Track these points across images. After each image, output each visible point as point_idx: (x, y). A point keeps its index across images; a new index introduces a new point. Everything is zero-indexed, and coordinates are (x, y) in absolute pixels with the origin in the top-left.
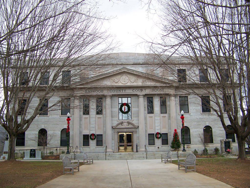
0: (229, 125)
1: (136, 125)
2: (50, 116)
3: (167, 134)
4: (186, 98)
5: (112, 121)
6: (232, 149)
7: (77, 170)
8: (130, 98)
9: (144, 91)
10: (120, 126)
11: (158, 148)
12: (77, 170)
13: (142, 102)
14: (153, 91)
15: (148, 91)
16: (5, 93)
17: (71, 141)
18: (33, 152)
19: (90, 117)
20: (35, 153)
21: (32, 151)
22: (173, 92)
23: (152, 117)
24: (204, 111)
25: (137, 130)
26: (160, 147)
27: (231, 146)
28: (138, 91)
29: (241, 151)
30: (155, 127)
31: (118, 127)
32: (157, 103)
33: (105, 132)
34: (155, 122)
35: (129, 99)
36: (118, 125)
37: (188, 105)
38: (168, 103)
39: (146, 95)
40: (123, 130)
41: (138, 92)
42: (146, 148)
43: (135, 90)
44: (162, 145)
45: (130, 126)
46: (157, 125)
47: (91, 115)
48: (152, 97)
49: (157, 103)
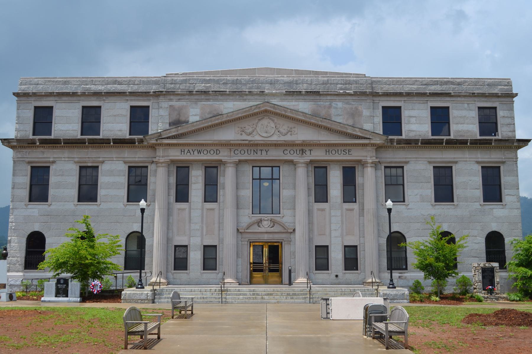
4: (399, 170)
9: (308, 153)
11: (335, 278)
15: (319, 155)
18: (63, 284)
21: (61, 284)
23: (323, 210)
25: (292, 236)
26: (340, 275)
33: (221, 241)
37: (403, 185)
39: (311, 162)
43: (288, 152)
45: (276, 229)
46: (333, 227)
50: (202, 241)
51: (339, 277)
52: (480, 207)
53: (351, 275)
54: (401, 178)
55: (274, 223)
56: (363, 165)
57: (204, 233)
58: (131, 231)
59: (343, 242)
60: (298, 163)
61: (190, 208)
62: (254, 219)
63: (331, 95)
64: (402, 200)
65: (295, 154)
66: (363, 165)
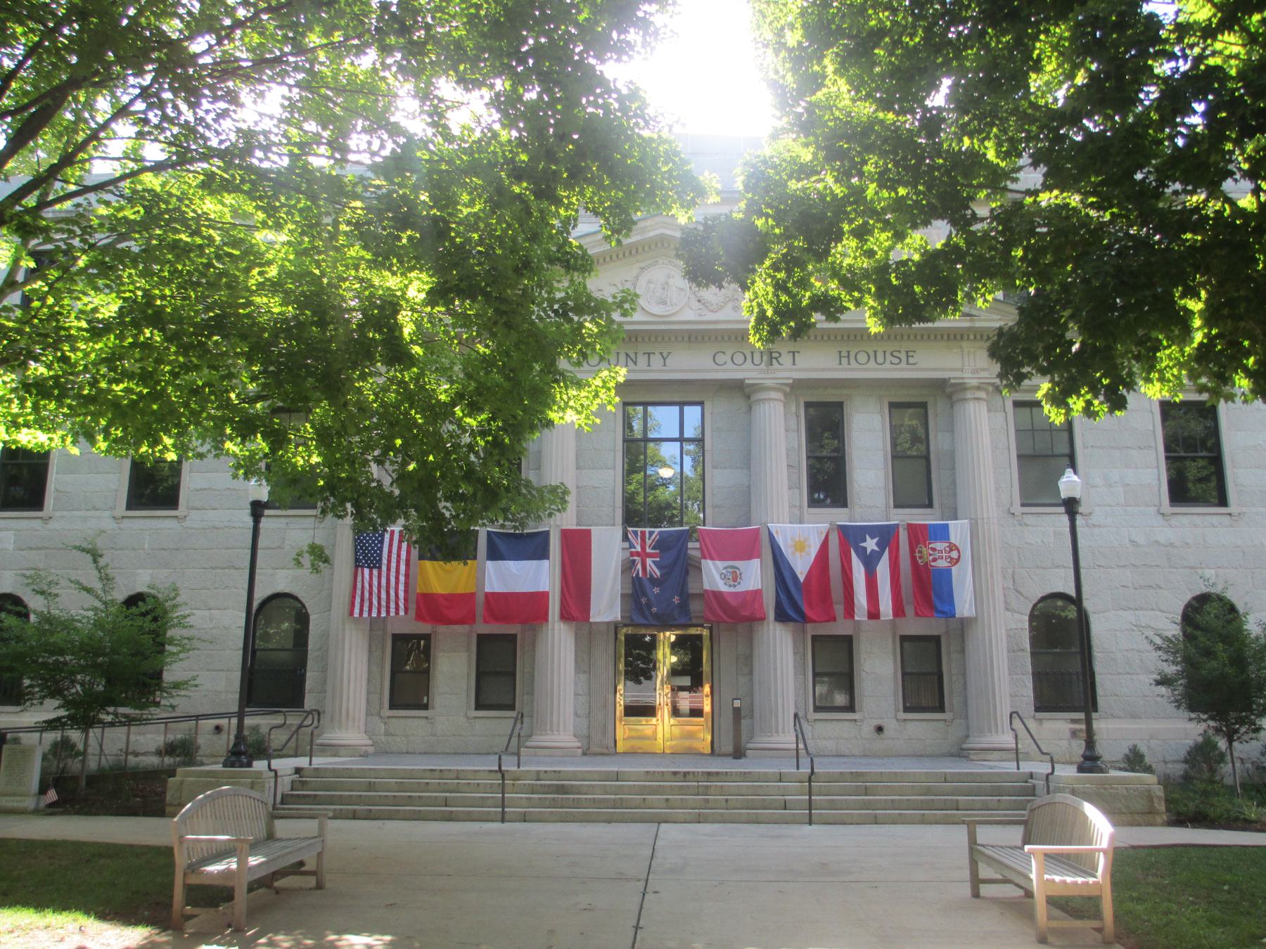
0: (1055, 590)
2: (193, 514)
7: (312, 881)
8: (699, 408)
9: (786, 359)
12: (312, 881)
14: (844, 360)
17: (312, 677)
22: (975, 371)
24: (1180, 492)
26: (891, 726)
28: (872, 359)
29: (224, 854)
35: (693, 413)
38: (938, 441)
39: (797, 386)
41: (749, 364)
42: (800, 735)
43: (727, 358)
44: (902, 715)
48: (840, 405)
56: (950, 397)
65: (872, 364)
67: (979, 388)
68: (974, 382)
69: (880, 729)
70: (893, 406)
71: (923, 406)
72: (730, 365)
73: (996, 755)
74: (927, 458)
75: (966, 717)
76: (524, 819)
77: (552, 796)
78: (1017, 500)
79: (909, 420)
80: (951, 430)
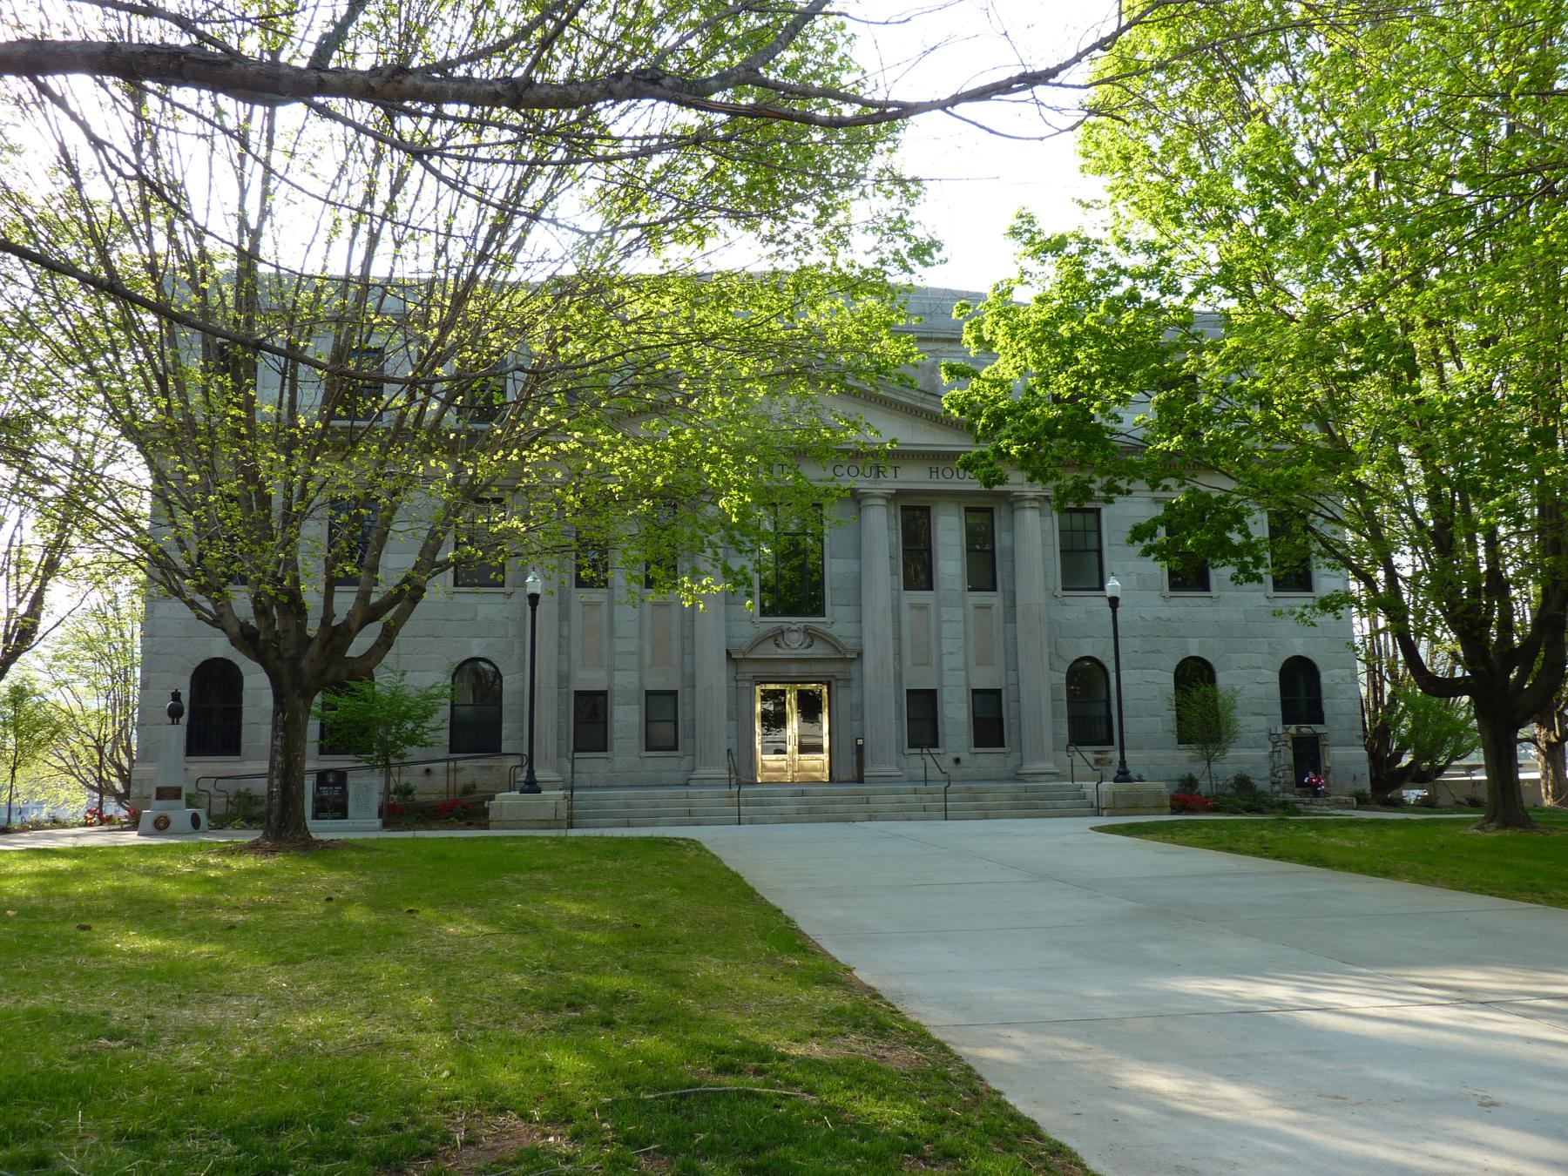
1: (850, 643)
3: (998, 692)
4: (1090, 518)
5: (727, 620)
6: (1327, 772)
9: (890, 473)
10: (769, 651)
11: (953, 764)
13: (881, 528)
15: (914, 478)
16: (86, 44)
18: (333, 785)
19: (611, 603)
20: (344, 793)
21: (328, 785)
23: (923, 607)
25: (854, 668)
26: (965, 756)
27: (1327, 763)
30: (941, 656)
31: (759, 654)
32: (949, 534)
33: (691, 680)
34: (939, 630)
36: (759, 641)
37: (1099, 551)
38: (1002, 539)
39: (900, 493)
40: (781, 670)
43: (844, 470)
44: (974, 750)
45: (819, 650)
46: (947, 646)
47: (616, 591)
48: (927, 510)
49: (949, 534)
50: (641, 679)
51: (964, 763)
52: (1266, 602)
53: (988, 760)
54: (1094, 536)
55: (811, 635)
56: (1011, 504)
57: (647, 662)
58: (466, 657)
59: (967, 680)
60: (1022, 498)
61: (611, 603)
62: (764, 628)
63: (938, 340)
64: (1097, 585)
65: (955, 478)
66: (1011, 504)
67: (1034, 499)
68: (1031, 495)
69: (957, 760)
70: (968, 510)
71: (991, 510)
72: (846, 477)
73: (1044, 778)
74: (993, 551)
75: (1021, 751)
76: (751, 822)
77: (553, 833)
78: (1059, 586)
79: (978, 519)
80: (1012, 531)
